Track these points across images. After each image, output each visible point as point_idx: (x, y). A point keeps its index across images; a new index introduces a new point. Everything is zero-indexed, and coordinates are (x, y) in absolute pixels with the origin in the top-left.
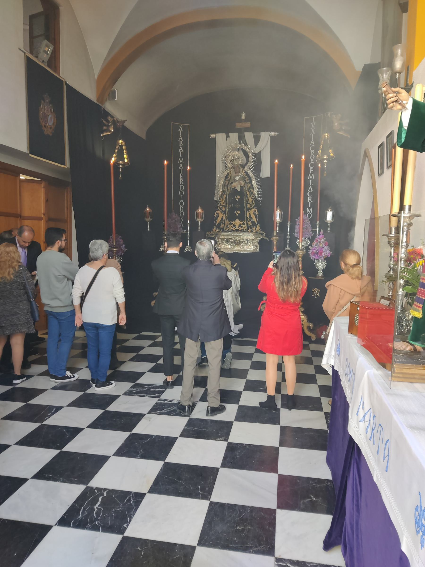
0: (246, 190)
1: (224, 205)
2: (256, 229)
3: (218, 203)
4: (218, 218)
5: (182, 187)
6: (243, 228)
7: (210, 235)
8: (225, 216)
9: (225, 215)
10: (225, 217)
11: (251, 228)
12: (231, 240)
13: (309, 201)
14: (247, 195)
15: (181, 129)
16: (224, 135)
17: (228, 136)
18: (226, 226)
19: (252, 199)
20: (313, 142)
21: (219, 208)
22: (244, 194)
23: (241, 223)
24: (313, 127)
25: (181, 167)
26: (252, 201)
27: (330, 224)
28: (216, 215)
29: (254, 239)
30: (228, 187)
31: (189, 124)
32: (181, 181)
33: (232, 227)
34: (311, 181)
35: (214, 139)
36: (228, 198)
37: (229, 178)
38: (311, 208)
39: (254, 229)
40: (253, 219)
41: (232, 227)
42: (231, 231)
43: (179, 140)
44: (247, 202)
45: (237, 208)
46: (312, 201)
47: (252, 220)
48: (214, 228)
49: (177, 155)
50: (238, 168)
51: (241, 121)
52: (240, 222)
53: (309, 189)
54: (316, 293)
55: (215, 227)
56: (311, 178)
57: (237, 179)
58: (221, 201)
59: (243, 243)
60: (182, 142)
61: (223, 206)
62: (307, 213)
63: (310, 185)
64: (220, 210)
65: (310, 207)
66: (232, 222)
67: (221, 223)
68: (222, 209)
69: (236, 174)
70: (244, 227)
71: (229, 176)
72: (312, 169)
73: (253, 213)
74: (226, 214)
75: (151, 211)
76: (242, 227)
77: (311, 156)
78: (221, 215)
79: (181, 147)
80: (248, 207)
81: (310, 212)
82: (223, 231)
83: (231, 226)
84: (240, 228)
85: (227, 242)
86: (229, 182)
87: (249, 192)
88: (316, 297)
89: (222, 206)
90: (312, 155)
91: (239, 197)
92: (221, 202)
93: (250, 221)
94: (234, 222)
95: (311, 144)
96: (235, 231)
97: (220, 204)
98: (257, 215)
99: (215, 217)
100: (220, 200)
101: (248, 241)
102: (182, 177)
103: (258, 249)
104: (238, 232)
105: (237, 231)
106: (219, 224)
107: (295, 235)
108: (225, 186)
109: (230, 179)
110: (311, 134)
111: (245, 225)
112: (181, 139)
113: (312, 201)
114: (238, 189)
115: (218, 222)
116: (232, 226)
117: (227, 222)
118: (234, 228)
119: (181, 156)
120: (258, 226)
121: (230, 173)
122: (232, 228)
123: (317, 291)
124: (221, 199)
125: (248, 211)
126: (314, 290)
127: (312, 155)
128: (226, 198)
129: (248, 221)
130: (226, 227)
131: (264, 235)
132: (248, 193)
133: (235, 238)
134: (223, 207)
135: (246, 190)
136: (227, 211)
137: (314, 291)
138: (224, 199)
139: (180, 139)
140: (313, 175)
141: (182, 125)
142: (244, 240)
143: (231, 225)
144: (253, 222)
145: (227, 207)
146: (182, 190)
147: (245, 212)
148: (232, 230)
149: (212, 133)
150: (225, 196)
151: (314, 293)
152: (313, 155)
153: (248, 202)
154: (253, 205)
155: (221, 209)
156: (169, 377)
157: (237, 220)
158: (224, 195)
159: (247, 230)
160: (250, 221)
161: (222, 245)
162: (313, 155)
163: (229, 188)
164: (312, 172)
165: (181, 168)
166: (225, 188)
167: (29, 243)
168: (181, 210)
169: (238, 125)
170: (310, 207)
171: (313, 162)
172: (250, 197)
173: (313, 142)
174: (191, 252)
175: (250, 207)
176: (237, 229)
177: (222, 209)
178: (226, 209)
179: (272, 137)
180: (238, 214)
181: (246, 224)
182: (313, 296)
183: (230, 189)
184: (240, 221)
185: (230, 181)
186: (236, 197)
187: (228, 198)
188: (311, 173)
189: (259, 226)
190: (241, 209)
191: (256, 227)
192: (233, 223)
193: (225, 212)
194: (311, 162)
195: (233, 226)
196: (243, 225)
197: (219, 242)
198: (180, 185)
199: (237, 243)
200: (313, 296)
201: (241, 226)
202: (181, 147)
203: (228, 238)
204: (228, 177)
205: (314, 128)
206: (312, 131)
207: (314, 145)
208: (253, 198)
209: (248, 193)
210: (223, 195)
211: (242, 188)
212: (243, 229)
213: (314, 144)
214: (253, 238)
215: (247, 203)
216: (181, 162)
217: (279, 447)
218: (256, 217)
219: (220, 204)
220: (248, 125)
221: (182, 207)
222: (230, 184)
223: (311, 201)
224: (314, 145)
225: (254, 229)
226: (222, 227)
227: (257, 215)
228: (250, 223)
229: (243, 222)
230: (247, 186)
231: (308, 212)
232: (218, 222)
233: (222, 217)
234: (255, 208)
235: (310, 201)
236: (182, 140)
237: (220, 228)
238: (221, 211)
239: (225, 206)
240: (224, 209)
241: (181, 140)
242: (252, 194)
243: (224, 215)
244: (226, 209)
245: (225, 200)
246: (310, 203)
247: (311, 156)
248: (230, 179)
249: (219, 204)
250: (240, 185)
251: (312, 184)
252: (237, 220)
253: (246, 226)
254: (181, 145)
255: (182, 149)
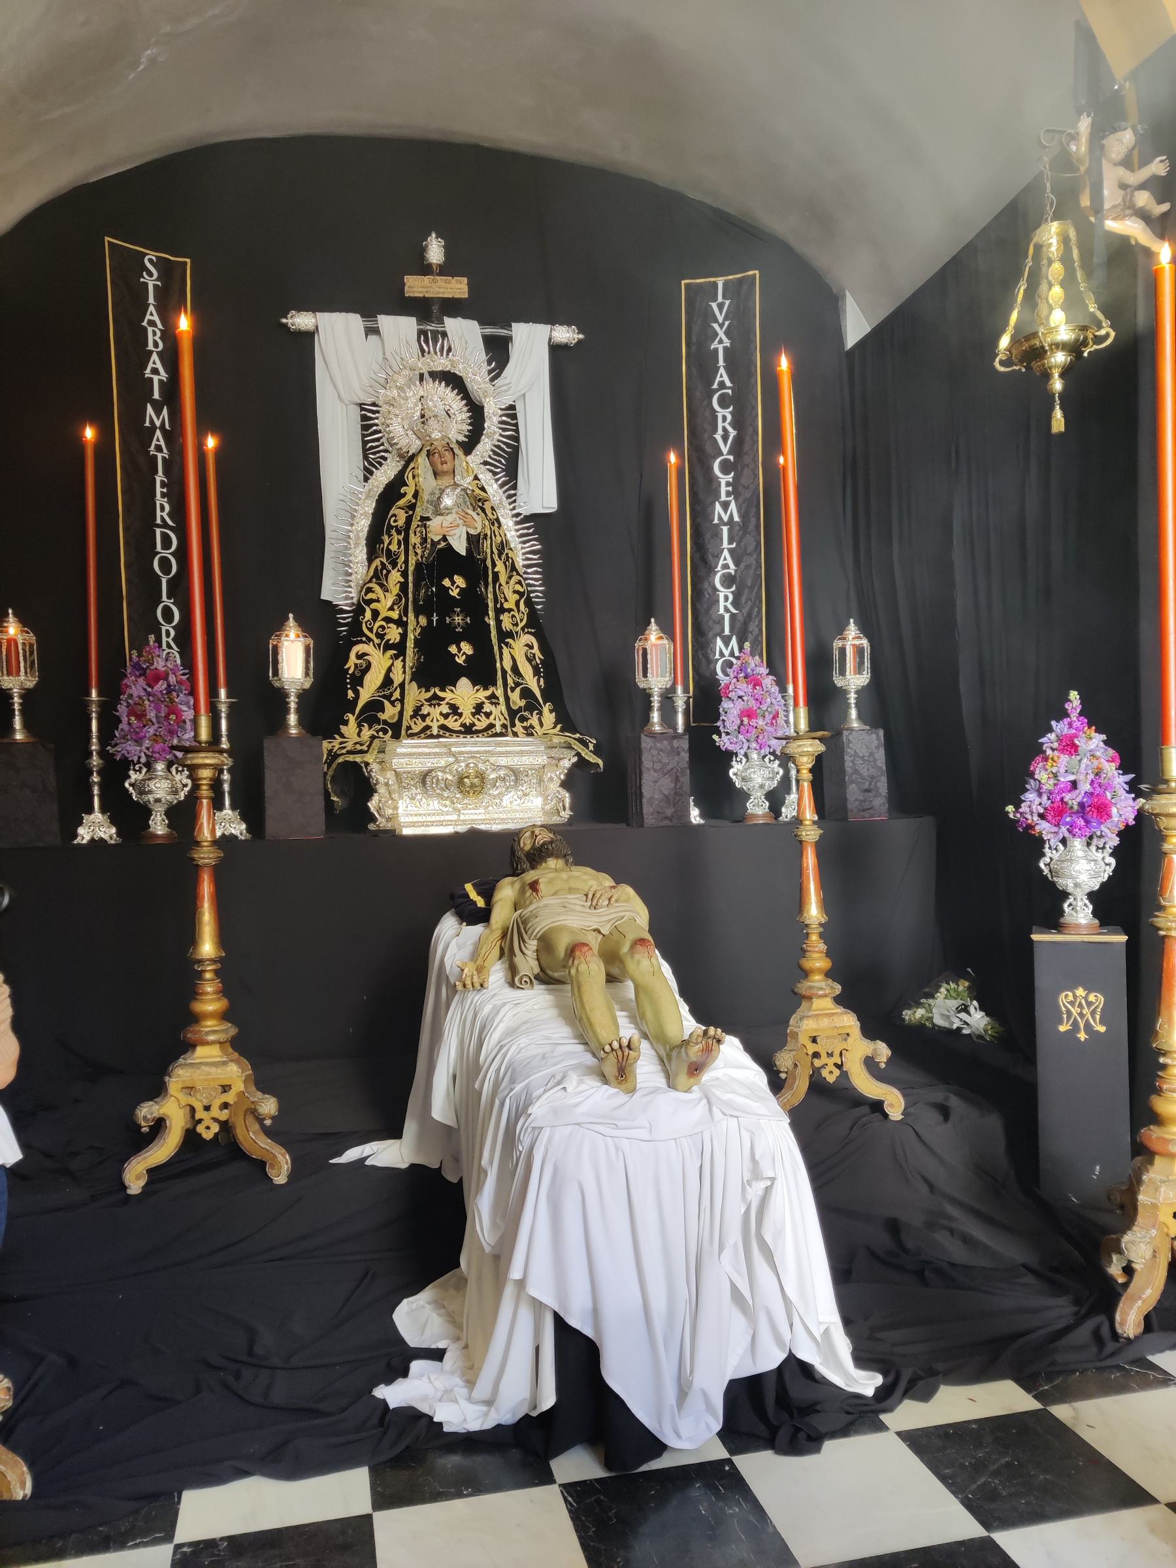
0: (492, 552)
1: (395, 615)
2: (541, 725)
3: (364, 611)
4: (368, 678)
5: (165, 538)
6: (492, 717)
7: (350, 752)
8: (404, 667)
9: (404, 661)
10: (401, 671)
11: (523, 719)
12: (440, 774)
13: (722, 611)
14: (496, 576)
15: (150, 274)
16: (353, 322)
17: (372, 331)
18: (409, 711)
19: (515, 592)
20: (723, 376)
21: (371, 630)
22: (486, 568)
23: (483, 694)
24: (720, 318)
25: (160, 446)
26: (517, 603)
27: (857, 692)
28: (356, 665)
29: (544, 766)
30: (412, 535)
31: (188, 261)
32: (163, 510)
33: (446, 716)
34: (725, 529)
35: (307, 338)
36: (411, 585)
37: (409, 497)
38: (734, 638)
39: (534, 720)
40: (527, 677)
41: (446, 716)
42: (441, 733)
43: (145, 324)
44: (499, 606)
45: (459, 630)
46: (734, 611)
47: (522, 684)
48: (346, 723)
49: (138, 390)
50: (448, 456)
51: (425, 269)
52: (478, 690)
53: (721, 562)
54: (1081, 1015)
55: (352, 718)
56: (726, 518)
57: (448, 501)
58: (378, 601)
59: (498, 784)
60: (159, 334)
61: (388, 620)
62: (717, 656)
63: (725, 544)
64: (377, 641)
65: (727, 632)
66: (443, 690)
67: (384, 697)
68: (387, 637)
69: (439, 482)
70: (498, 714)
71: (404, 488)
72: (728, 484)
73: (523, 653)
74: (407, 659)
75: (32, 638)
76: (488, 715)
77: (720, 431)
78: (380, 662)
79: (155, 357)
80: (504, 628)
81: (732, 654)
82: (396, 736)
83: (438, 710)
84: (479, 720)
85: (424, 782)
86: (411, 513)
87: (505, 563)
88: (1082, 1036)
89: (383, 620)
90: (724, 429)
91: (460, 581)
92: (374, 605)
93: (518, 690)
94: (452, 691)
95: (715, 386)
96: (460, 732)
97: (376, 614)
98: (539, 662)
99: (350, 672)
100: (370, 596)
101: (516, 775)
102: (165, 490)
103: (564, 809)
104: (478, 737)
105: (468, 730)
106: (375, 706)
107: (724, 742)
108: (393, 532)
109: (414, 501)
110: (712, 347)
111: (499, 704)
112: (156, 318)
113: (734, 611)
114: (461, 547)
115: (367, 692)
116: (444, 712)
117: (415, 693)
118: (456, 720)
119: (156, 396)
120: (546, 708)
121: (414, 477)
122: (442, 721)
123: (1089, 1004)
124: (377, 588)
125: (507, 644)
126: (1071, 998)
127: (724, 429)
128: (404, 587)
129: (509, 686)
130: (412, 717)
131: (591, 747)
132: (500, 567)
133: (463, 764)
134: (390, 625)
135: (492, 552)
136: (410, 644)
137: (1072, 1003)
138: (396, 590)
139: (148, 317)
140: (733, 506)
141: (154, 259)
142: (502, 773)
143: (439, 705)
144: (527, 693)
145: (410, 627)
146: (167, 554)
147: (496, 648)
148: (443, 727)
149: (301, 308)
150: (395, 577)
151: (1069, 1013)
152: (730, 429)
153: (502, 604)
154: (521, 620)
155: (380, 636)
156: (8, 1400)
157: (464, 683)
158: (389, 572)
159: (509, 729)
160: (518, 690)
161: (401, 797)
162: (730, 429)
163: (414, 539)
164: (728, 494)
165: (159, 448)
166: (396, 541)
167: (930, 1019)
168: (167, 642)
169: (416, 286)
170: (727, 632)
171: (729, 453)
172: (507, 583)
173: (723, 376)
174: (113, 842)
175: (511, 627)
176: (468, 722)
177: (385, 634)
178: (404, 636)
179: (557, 351)
180: (464, 657)
181: (502, 700)
182: (1062, 1028)
183: (421, 544)
184: (476, 688)
185: (418, 510)
186: (446, 582)
187: (411, 585)
188: (723, 498)
189: (551, 712)
190: (478, 634)
191: (540, 713)
192: (447, 695)
193: (399, 649)
194: (723, 455)
195: (450, 708)
196: (492, 703)
197: (387, 784)
198: (159, 526)
199: (472, 786)
200: (1062, 1028)
201: (484, 711)
202: (155, 353)
203: (429, 764)
204: (405, 494)
205: (727, 323)
206: (716, 334)
207: (729, 388)
208: (518, 587)
209: (500, 567)
210: (385, 572)
211: (474, 541)
212: (493, 722)
213: (728, 384)
214: (542, 760)
215: (500, 611)
216: (158, 423)
217: (371, 1515)
218: (536, 671)
219: (376, 614)
220: (457, 288)
221: (172, 633)
222: (415, 524)
223: (730, 612)
224: (729, 388)
225: (534, 720)
226: (392, 717)
227: (539, 662)
228: (515, 697)
229: (488, 693)
230: (495, 536)
231: (722, 654)
232: (367, 692)
233: (389, 670)
234: (528, 633)
235: (727, 610)
236: (160, 326)
237: (378, 721)
238: (379, 645)
239: (401, 623)
240: (394, 634)
241: (152, 323)
242: (515, 573)
243: (398, 663)
244: (404, 636)
245: (398, 595)
246: (727, 616)
247: (720, 431)
248: (414, 501)
249: (368, 615)
250: (464, 529)
251: (730, 543)
252: (464, 683)
253: (503, 708)
254: (156, 345)
255: (159, 366)
